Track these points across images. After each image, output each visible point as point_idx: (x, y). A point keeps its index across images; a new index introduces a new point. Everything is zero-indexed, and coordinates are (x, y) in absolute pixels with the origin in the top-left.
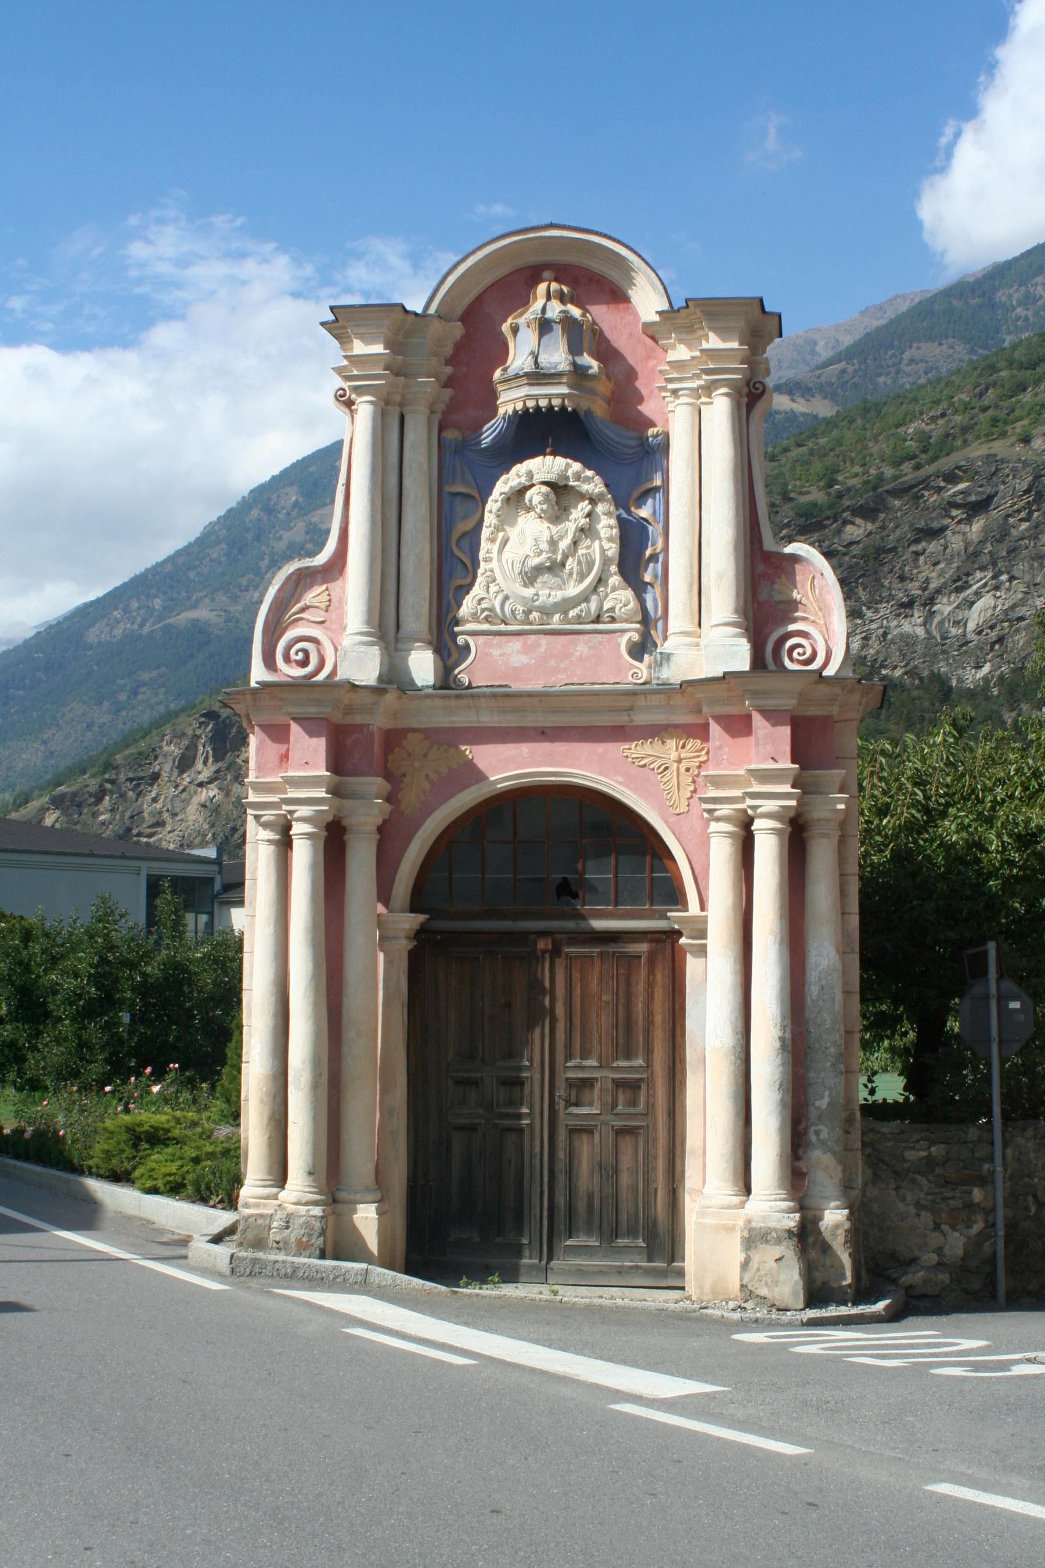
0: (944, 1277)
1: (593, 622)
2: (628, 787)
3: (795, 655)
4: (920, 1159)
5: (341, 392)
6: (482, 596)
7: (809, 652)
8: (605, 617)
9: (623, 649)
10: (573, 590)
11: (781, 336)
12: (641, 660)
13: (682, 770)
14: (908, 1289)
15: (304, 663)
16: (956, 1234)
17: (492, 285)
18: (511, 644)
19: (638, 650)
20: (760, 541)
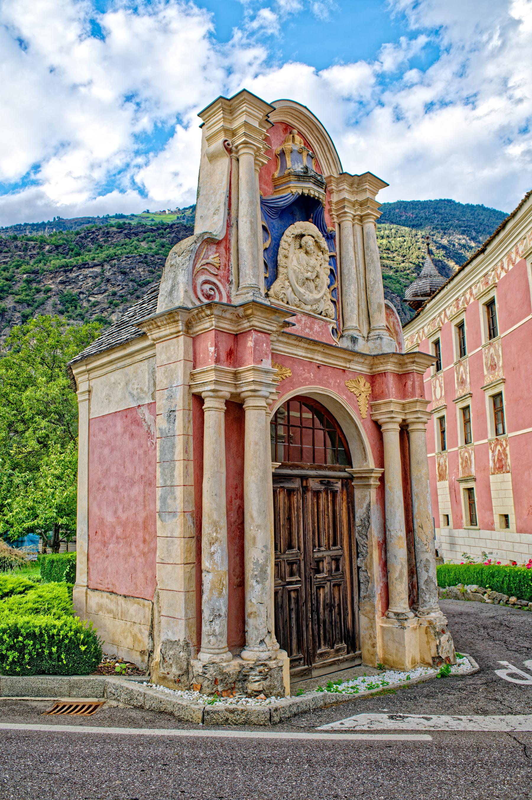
8: (323, 314)
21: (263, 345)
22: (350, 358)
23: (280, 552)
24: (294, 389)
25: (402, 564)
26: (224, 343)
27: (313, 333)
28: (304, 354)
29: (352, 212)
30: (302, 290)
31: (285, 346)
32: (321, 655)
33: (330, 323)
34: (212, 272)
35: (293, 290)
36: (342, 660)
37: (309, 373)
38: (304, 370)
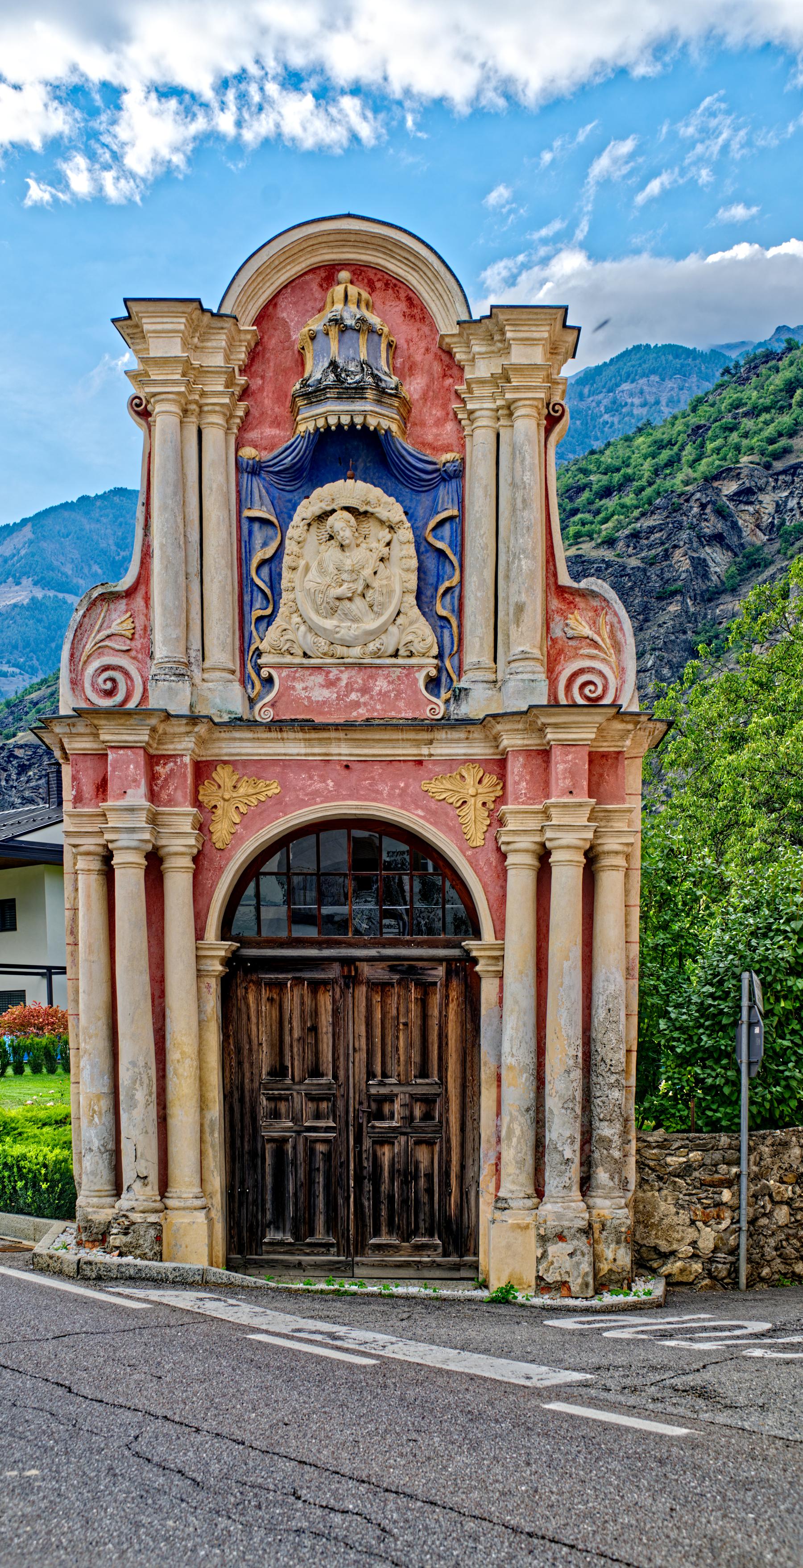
0: (697, 1267)
1: (391, 656)
2: (428, 821)
3: (586, 691)
4: (680, 1164)
5: (137, 401)
6: (284, 627)
7: (599, 691)
8: (402, 652)
9: (421, 684)
10: (372, 624)
11: (574, 357)
12: (438, 696)
13: (480, 805)
14: (668, 1276)
15: (109, 693)
16: (708, 1229)
17: (285, 287)
18: (312, 678)
19: (433, 684)
20: (555, 575)
21: (128, 767)
22: (426, 736)
23: (293, 1079)
24: (286, 814)
25: (511, 1114)
26: (91, 772)
27: (372, 698)
28: (303, 751)
29: (486, 406)
30: (329, 624)
31: (257, 744)
32: (379, 1247)
33: (421, 667)
34: (118, 647)
35: (310, 629)
36: (427, 1262)
37: (324, 782)
38: (311, 778)
